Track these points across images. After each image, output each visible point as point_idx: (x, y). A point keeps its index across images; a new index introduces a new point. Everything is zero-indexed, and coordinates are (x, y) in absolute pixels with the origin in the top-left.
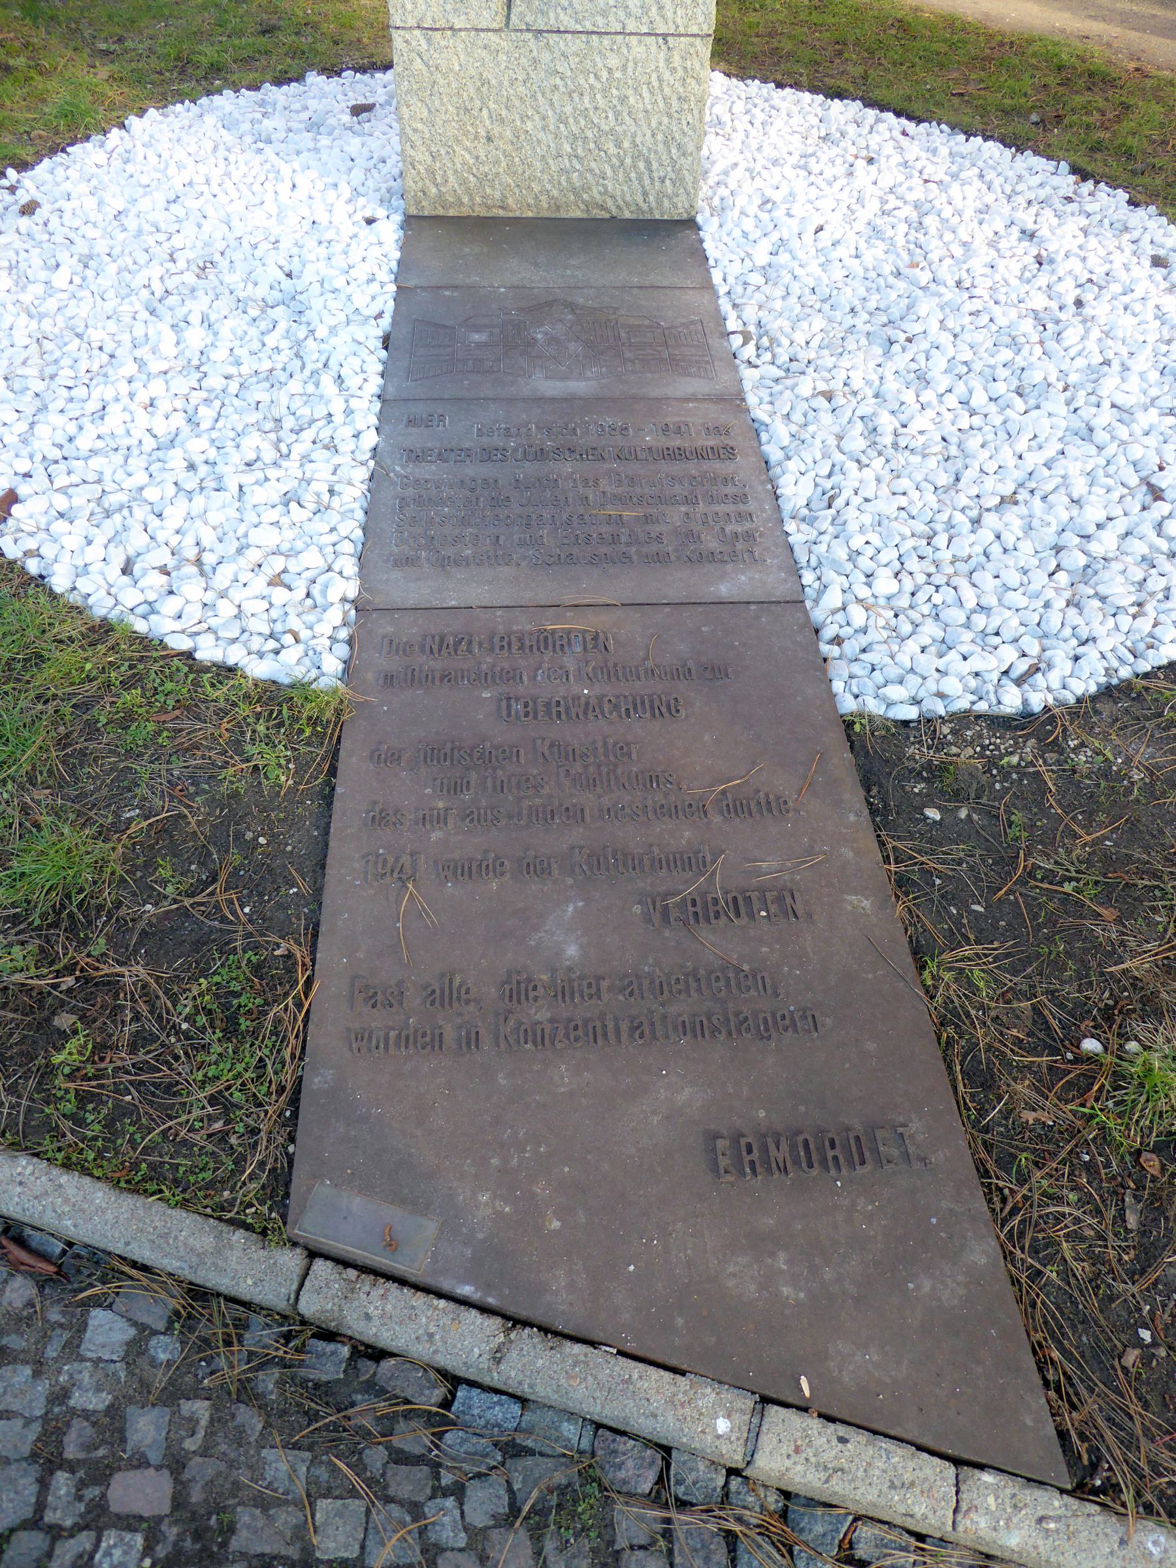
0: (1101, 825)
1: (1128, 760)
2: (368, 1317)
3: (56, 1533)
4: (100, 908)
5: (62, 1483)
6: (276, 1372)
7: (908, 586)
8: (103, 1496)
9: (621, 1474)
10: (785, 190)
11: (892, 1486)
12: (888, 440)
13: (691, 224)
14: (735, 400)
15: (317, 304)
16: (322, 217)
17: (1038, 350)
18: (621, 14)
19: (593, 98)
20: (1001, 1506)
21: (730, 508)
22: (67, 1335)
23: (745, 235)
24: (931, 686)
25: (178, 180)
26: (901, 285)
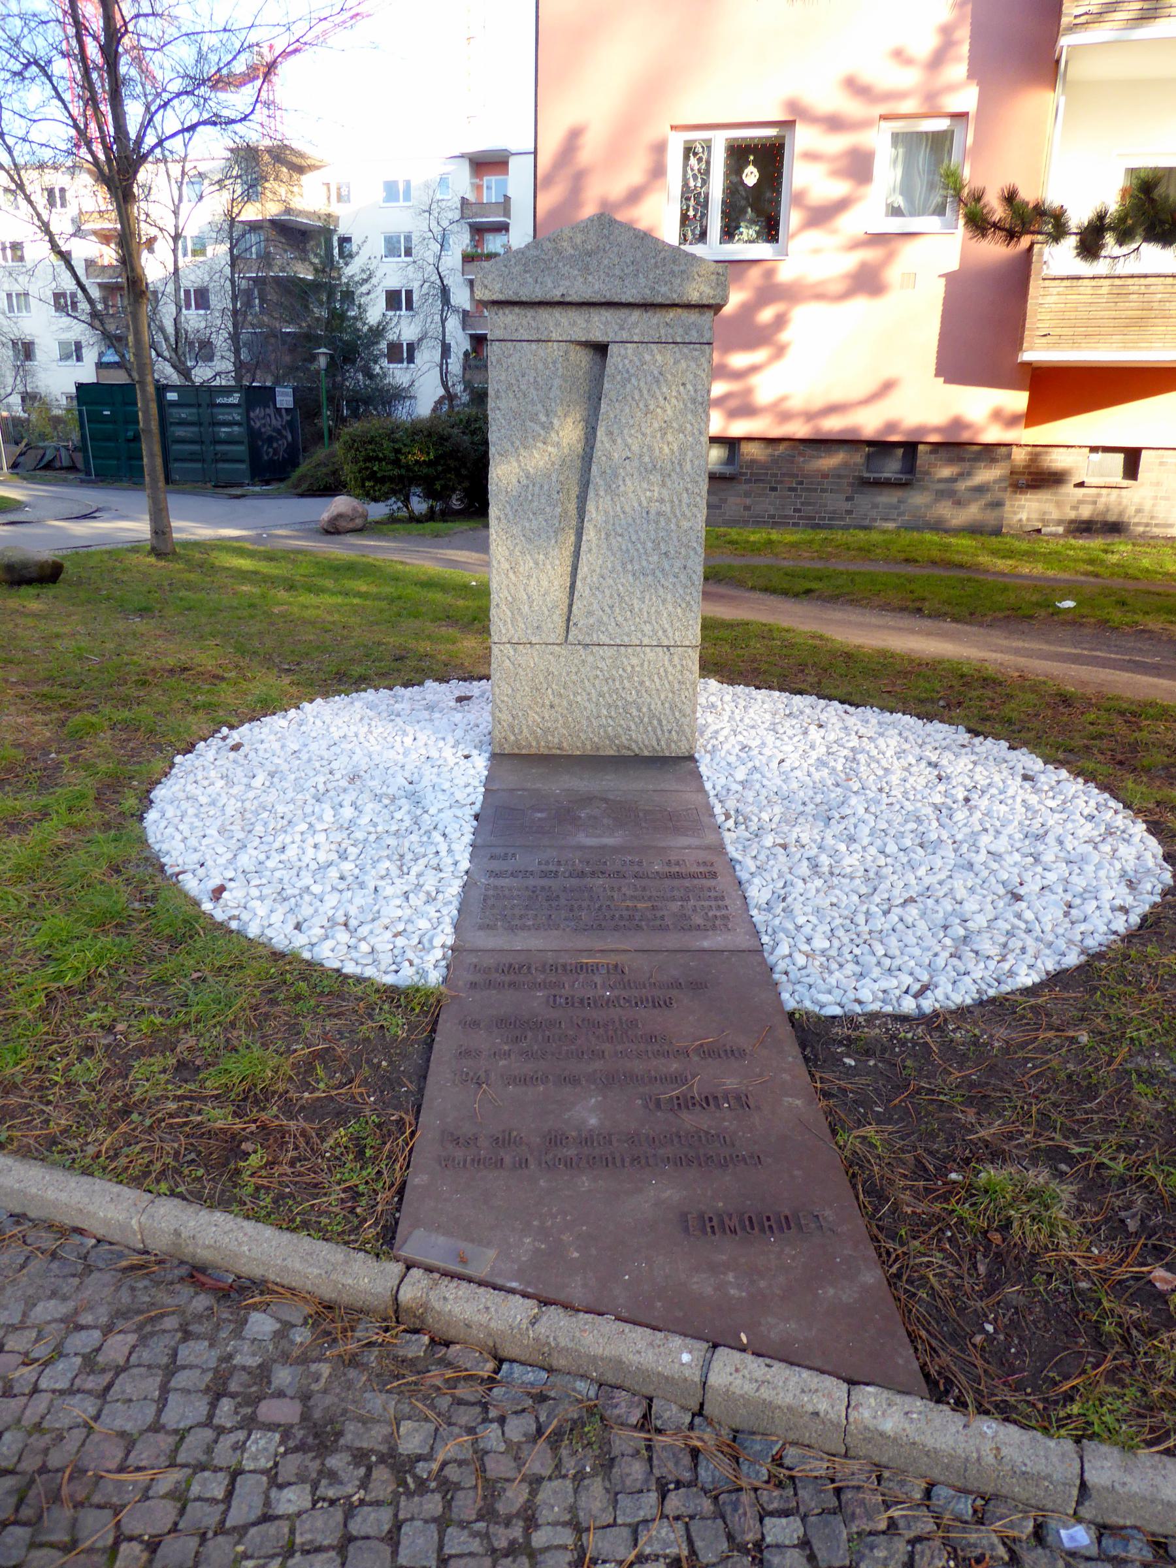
0: (969, 1068)
1: (991, 1037)
2: (445, 1299)
3: (221, 1431)
4: (275, 1092)
5: (226, 1405)
6: (376, 1351)
7: (836, 943)
8: (254, 1412)
9: (617, 1411)
10: (758, 742)
11: (803, 1391)
12: (826, 869)
13: (691, 758)
14: (720, 849)
15: (430, 796)
16: (434, 754)
17: (935, 824)
18: (639, 635)
19: (622, 682)
20: (879, 1404)
21: (713, 903)
22: (232, 1326)
23: (729, 764)
24: (851, 995)
25: (336, 735)
26: (839, 790)
